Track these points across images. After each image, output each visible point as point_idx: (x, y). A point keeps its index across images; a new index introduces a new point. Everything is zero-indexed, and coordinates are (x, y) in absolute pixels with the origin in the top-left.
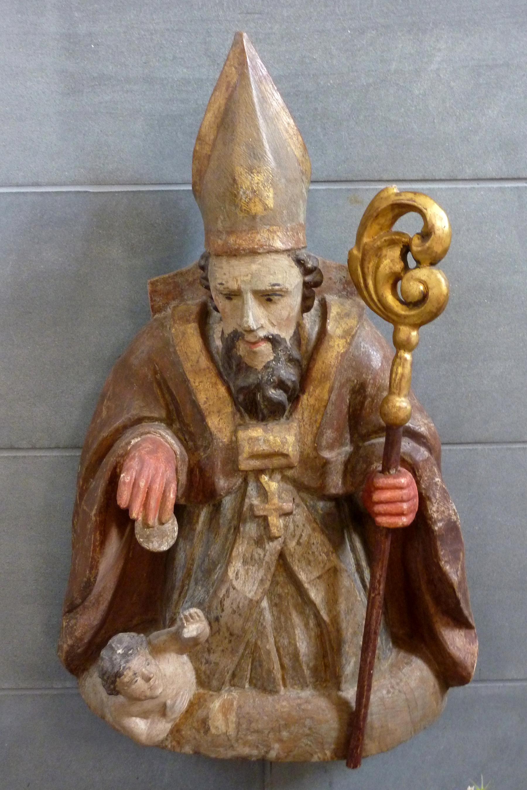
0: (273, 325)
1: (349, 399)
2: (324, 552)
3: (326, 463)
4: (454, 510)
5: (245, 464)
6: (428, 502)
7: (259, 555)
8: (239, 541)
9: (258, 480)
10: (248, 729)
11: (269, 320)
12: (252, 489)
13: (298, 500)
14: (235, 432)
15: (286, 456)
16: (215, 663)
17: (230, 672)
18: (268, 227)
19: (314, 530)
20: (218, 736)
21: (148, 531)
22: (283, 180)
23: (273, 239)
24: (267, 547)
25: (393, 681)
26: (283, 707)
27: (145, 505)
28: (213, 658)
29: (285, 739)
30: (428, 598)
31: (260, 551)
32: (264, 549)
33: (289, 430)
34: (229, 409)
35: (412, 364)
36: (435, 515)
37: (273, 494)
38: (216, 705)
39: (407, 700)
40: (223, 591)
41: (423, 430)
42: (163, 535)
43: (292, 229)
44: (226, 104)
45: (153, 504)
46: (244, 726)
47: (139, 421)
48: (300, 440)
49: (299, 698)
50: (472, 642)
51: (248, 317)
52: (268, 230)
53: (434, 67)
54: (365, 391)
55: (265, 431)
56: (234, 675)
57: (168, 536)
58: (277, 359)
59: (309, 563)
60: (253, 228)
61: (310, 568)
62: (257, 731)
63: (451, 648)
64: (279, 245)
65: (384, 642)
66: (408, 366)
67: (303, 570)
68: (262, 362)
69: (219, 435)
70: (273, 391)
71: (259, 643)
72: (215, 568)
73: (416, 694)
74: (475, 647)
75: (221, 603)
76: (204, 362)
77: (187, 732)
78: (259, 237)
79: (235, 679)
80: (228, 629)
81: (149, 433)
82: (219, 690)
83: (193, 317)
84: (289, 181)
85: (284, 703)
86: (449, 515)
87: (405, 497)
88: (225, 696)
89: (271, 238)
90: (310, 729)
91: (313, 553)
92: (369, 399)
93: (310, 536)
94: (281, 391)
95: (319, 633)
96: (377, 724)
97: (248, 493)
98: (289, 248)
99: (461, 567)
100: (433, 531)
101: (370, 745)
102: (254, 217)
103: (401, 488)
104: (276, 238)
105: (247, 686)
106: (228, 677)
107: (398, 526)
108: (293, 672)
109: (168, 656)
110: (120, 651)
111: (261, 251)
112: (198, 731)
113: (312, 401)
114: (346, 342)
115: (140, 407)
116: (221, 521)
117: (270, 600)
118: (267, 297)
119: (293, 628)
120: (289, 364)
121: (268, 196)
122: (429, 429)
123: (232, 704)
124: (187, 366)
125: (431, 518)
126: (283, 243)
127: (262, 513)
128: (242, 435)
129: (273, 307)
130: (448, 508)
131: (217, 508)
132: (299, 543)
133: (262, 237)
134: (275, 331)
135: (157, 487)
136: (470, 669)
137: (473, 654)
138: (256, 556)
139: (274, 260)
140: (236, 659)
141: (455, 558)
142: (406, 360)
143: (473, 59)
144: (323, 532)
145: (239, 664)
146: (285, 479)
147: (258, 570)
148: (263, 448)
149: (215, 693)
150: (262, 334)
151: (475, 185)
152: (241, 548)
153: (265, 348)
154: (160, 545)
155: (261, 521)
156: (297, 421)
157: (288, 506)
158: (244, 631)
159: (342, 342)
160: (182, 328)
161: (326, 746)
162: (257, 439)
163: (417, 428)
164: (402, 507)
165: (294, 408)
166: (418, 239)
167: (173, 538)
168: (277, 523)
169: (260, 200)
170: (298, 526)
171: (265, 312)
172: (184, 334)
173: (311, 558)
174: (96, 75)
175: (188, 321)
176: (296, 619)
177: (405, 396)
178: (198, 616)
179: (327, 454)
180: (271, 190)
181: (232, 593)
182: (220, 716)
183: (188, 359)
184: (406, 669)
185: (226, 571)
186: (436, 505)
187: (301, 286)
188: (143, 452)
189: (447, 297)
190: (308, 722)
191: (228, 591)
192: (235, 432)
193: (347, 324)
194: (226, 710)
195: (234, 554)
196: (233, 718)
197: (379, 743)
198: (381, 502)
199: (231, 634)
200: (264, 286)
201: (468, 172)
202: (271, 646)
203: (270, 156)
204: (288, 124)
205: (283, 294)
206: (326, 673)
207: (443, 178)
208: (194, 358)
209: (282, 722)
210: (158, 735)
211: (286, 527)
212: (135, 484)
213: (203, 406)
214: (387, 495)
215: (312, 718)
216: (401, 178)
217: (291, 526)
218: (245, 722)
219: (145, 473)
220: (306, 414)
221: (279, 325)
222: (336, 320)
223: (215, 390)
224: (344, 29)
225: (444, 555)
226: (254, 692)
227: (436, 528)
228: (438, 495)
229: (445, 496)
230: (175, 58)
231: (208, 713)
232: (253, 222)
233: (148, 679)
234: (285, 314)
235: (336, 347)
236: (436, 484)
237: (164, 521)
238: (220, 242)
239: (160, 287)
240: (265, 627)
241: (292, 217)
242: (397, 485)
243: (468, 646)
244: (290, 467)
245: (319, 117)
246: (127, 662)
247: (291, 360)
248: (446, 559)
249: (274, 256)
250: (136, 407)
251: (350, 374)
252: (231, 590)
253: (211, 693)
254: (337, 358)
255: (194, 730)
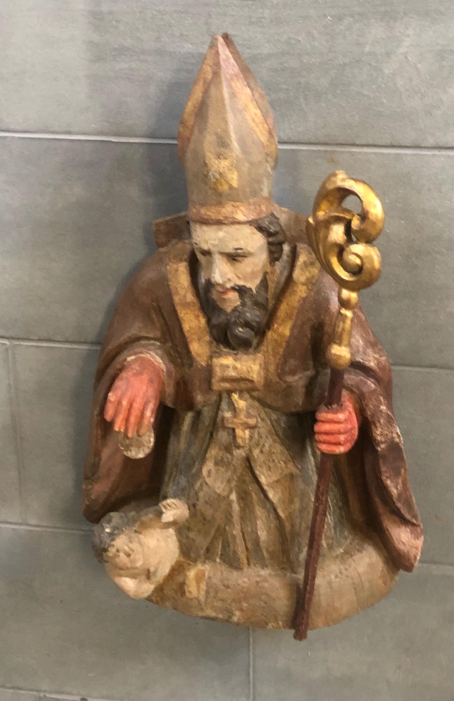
0: (239, 278)
1: (310, 334)
2: (282, 460)
3: (289, 387)
4: (397, 433)
5: (217, 386)
6: (373, 427)
7: (228, 458)
8: (213, 445)
9: (229, 396)
10: (215, 597)
11: (236, 274)
12: (224, 405)
13: (263, 415)
14: (211, 358)
15: (252, 381)
16: (192, 539)
17: (204, 548)
18: (232, 203)
19: (275, 441)
20: (191, 599)
21: (128, 442)
22: (247, 165)
23: (236, 212)
24: (234, 452)
25: (342, 567)
26: (244, 582)
27: (127, 420)
28: (192, 535)
29: (244, 608)
30: (377, 500)
31: (229, 456)
32: (232, 454)
33: (254, 360)
34: (208, 338)
35: (352, 320)
36: (379, 438)
37: (241, 410)
38: (192, 574)
39: (354, 583)
40: (198, 484)
41: (372, 364)
42: (140, 445)
43: (254, 204)
44: (203, 97)
45: (132, 419)
46: (212, 595)
47: (139, 339)
48: (265, 367)
49: (259, 576)
50: (417, 537)
51: (215, 273)
52: (233, 206)
53: (402, 50)
54: (323, 329)
55: (236, 360)
56: (208, 550)
57: (144, 446)
58: (243, 304)
59: (269, 468)
60: (220, 204)
61: (269, 473)
62: (222, 600)
63: (396, 542)
64: (240, 217)
65: (338, 533)
66: (348, 322)
67: (263, 474)
68: (230, 306)
69: (198, 359)
70: (241, 329)
71: (227, 528)
72: (194, 464)
73: (363, 578)
74: (420, 543)
75: (196, 494)
76: (190, 297)
77: (168, 592)
78: (224, 210)
79: (209, 555)
80: (202, 514)
81: (142, 353)
82: (195, 561)
83: (186, 256)
84: (251, 163)
85: (246, 580)
86: (393, 438)
87: (342, 431)
88: (200, 566)
89: (234, 212)
90: (265, 603)
91: (273, 461)
92: (327, 336)
93: (271, 446)
94: (248, 329)
95: (278, 525)
96: (324, 603)
97: (221, 407)
98: (250, 219)
99: (402, 481)
100: (377, 451)
101: (317, 619)
102: (220, 195)
103: (339, 422)
104: (238, 211)
105: (218, 560)
106: (202, 552)
107: (335, 453)
108: (255, 552)
109: (152, 531)
110: (108, 530)
111: (226, 222)
112: (176, 593)
113: (275, 336)
114: (308, 288)
115: (139, 327)
116: (200, 426)
117: (238, 494)
118: (234, 257)
119: (256, 518)
120: (255, 307)
121: (233, 178)
122: (379, 363)
123: (204, 575)
124: (176, 299)
125: (375, 440)
126: (245, 216)
127: (230, 426)
128: (215, 361)
129: (238, 265)
130: (392, 432)
131: (199, 414)
132: (262, 452)
133: (227, 210)
134: (241, 283)
135: (137, 406)
136: (413, 561)
137: (417, 549)
138: (225, 460)
139: (237, 229)
140: (209, 540)
141: (397, 473)
142: (346, 316)
143: (437, 44)
144: (283, 444)
145: (212, 542)
146: (253, 397)
147: (226, 472)
148: (232, 373)
149: (191, 563)
150: (228, 286)
151: (436, 152)
152: (213, 452)
153: (233, 296)
154: (137, 453)
155: (231, 432)
156: (262, 352)
157: (252, 422)
158: (214, 518)
159: (304, 288)
160: (175, 266)
161: (279, 618)
162: (228, 367)
163: (366, 363)
164: (339, 438)
165: (259, 344)
166: (358, 219)
167: (149, 448)
168: (243, 434)
169: (225, 180)
170: (261, 437)
171: (232, 268)
172: (177, 270)
173: (271, 465)
174: (117, 47)
175: (181, 260)
176: (259, 512)
177: (345, 346)
178: (175, 505)
179: (290, 379)
180: (235, 173)
181: (205, 488)
182: (194, 583)
183: (178, 293)
184: (357, 556)
185: (201, 469)
186: (380, 430)
187: (266, 246)
188: (130, 373)
189: (379, 271)
190: (263, 597)
191: (201, 485)
192: (211, 358)
193: (310, 272)
194: (199, 578)
195: (207, 456)
196: (203, 586)
197: (325, 618)
198: (320, 433)
199: (205, 519)
200: (230, 249)
201: (431, 141)
202: (237, 531)
203: (235, 145)
204: (255, 114)
205: (246, 255)
206: (282, 556)
207: (408, 145)
208: (182, 292)
209: (242, 595)
210: (143, 593)
211: (251, 437)
212: (119, 403)
213: (187, 334)
214: (327, 427)
215: (267, 594)
216: (371, 142)
217: (256, 436)
218: (212, 591)
219: (129, 393)
220: (270, 347)
221: (245, 279)
222: (302, 269)
223: (197, 321)
224: (325, 16)
225: (385, 472)
226: (224, 567)
227: (379, 449)
228: (382, 421)
229: (390, 421)
230: (182, 35)
231: (184, 580)
232: (219, 198)
233: (128, 555)
234: (249, 270)
235: (299, 292)
236: (381, 411)
237: (141, 434)
238: (194, 210)
239: (162, 228)
240: (232, 516)
241: (255, 193)
242: (335, 420)
243: (413, 541)
244: (255, 389)
245: (302, 90)
246: (113, 540)
247: (256, 304)
248: (388, 475)
249: (238, 226)
250: (136, 328)
251: (311, 315)
252: (204, 485)
253: (189, 562)
254: (299, 301)
255: (173, 591)
